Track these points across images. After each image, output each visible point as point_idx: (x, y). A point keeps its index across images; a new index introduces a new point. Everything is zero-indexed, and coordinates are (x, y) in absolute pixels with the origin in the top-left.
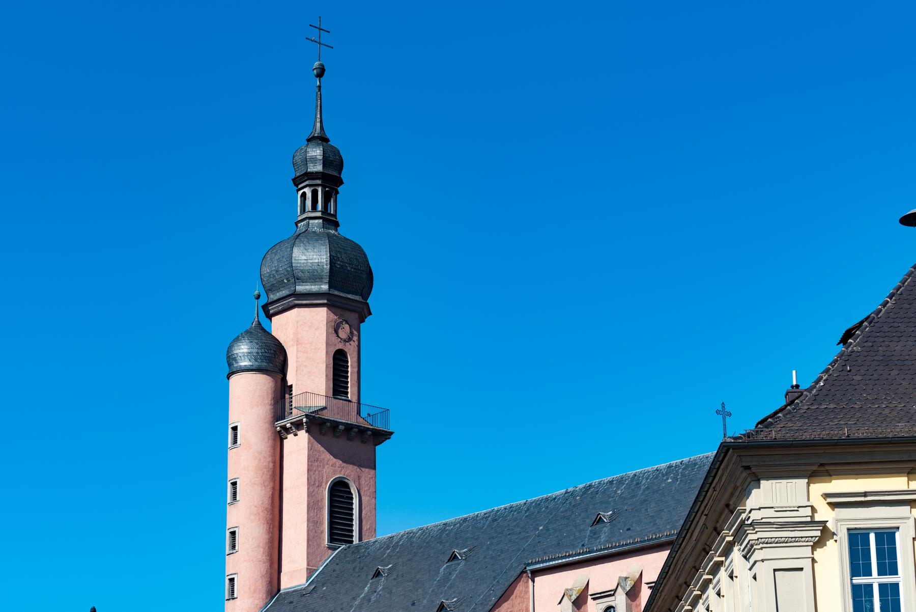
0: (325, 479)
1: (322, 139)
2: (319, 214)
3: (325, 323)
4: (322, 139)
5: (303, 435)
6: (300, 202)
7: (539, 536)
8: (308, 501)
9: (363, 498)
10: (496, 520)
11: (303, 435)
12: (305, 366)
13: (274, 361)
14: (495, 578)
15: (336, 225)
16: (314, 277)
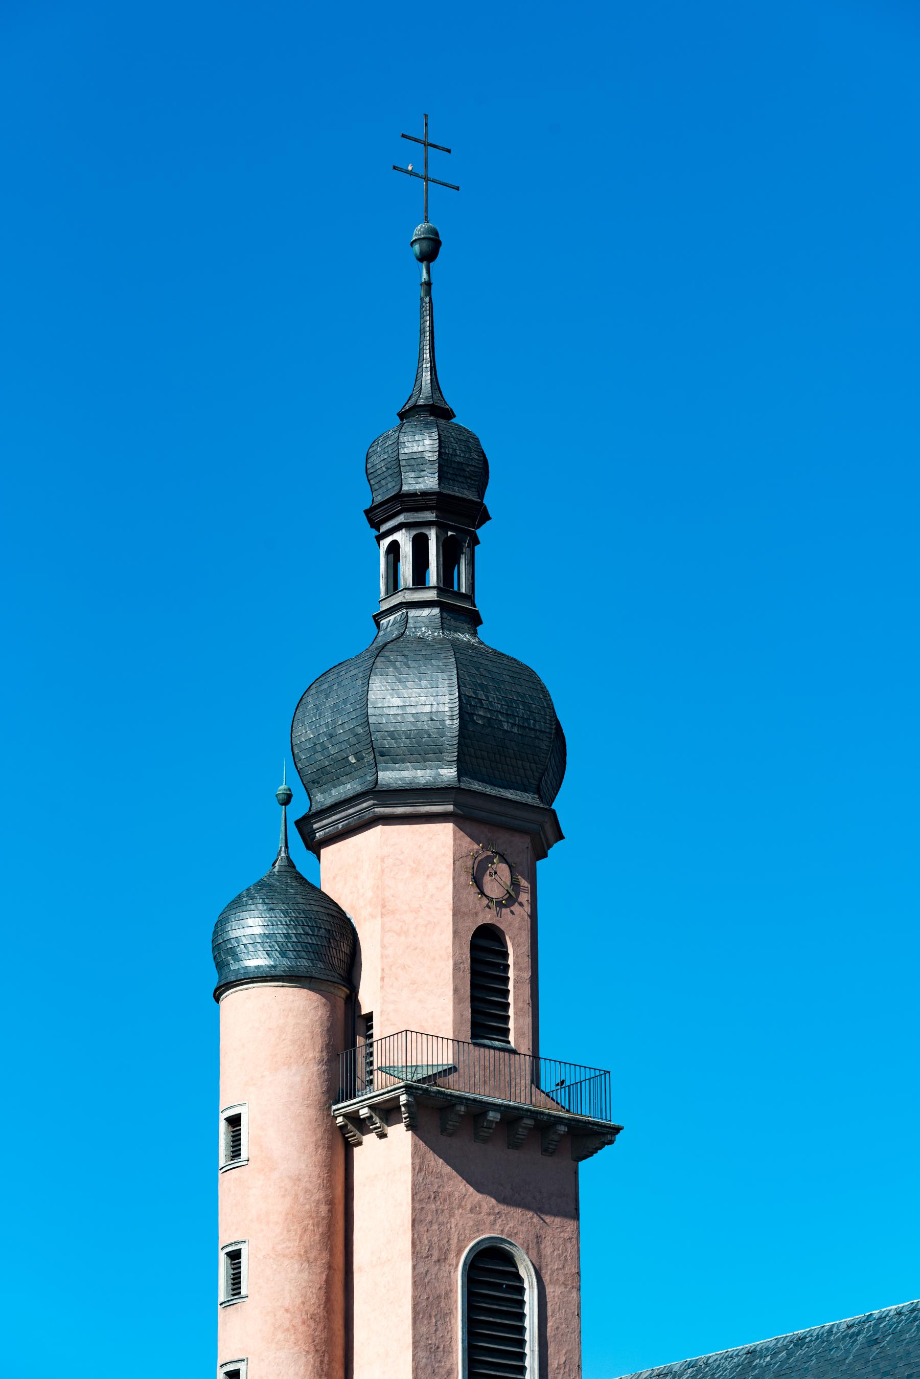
0: (454, 1242)
1: (436, 412)
2: (431, 595)
4: (436, 412)
8: (414, 1297)
9: (549, 1290)
10: (876, 1342)
12: (404, 967)
13: (326, 953)
15: (474, 619)
16: (422, 749)
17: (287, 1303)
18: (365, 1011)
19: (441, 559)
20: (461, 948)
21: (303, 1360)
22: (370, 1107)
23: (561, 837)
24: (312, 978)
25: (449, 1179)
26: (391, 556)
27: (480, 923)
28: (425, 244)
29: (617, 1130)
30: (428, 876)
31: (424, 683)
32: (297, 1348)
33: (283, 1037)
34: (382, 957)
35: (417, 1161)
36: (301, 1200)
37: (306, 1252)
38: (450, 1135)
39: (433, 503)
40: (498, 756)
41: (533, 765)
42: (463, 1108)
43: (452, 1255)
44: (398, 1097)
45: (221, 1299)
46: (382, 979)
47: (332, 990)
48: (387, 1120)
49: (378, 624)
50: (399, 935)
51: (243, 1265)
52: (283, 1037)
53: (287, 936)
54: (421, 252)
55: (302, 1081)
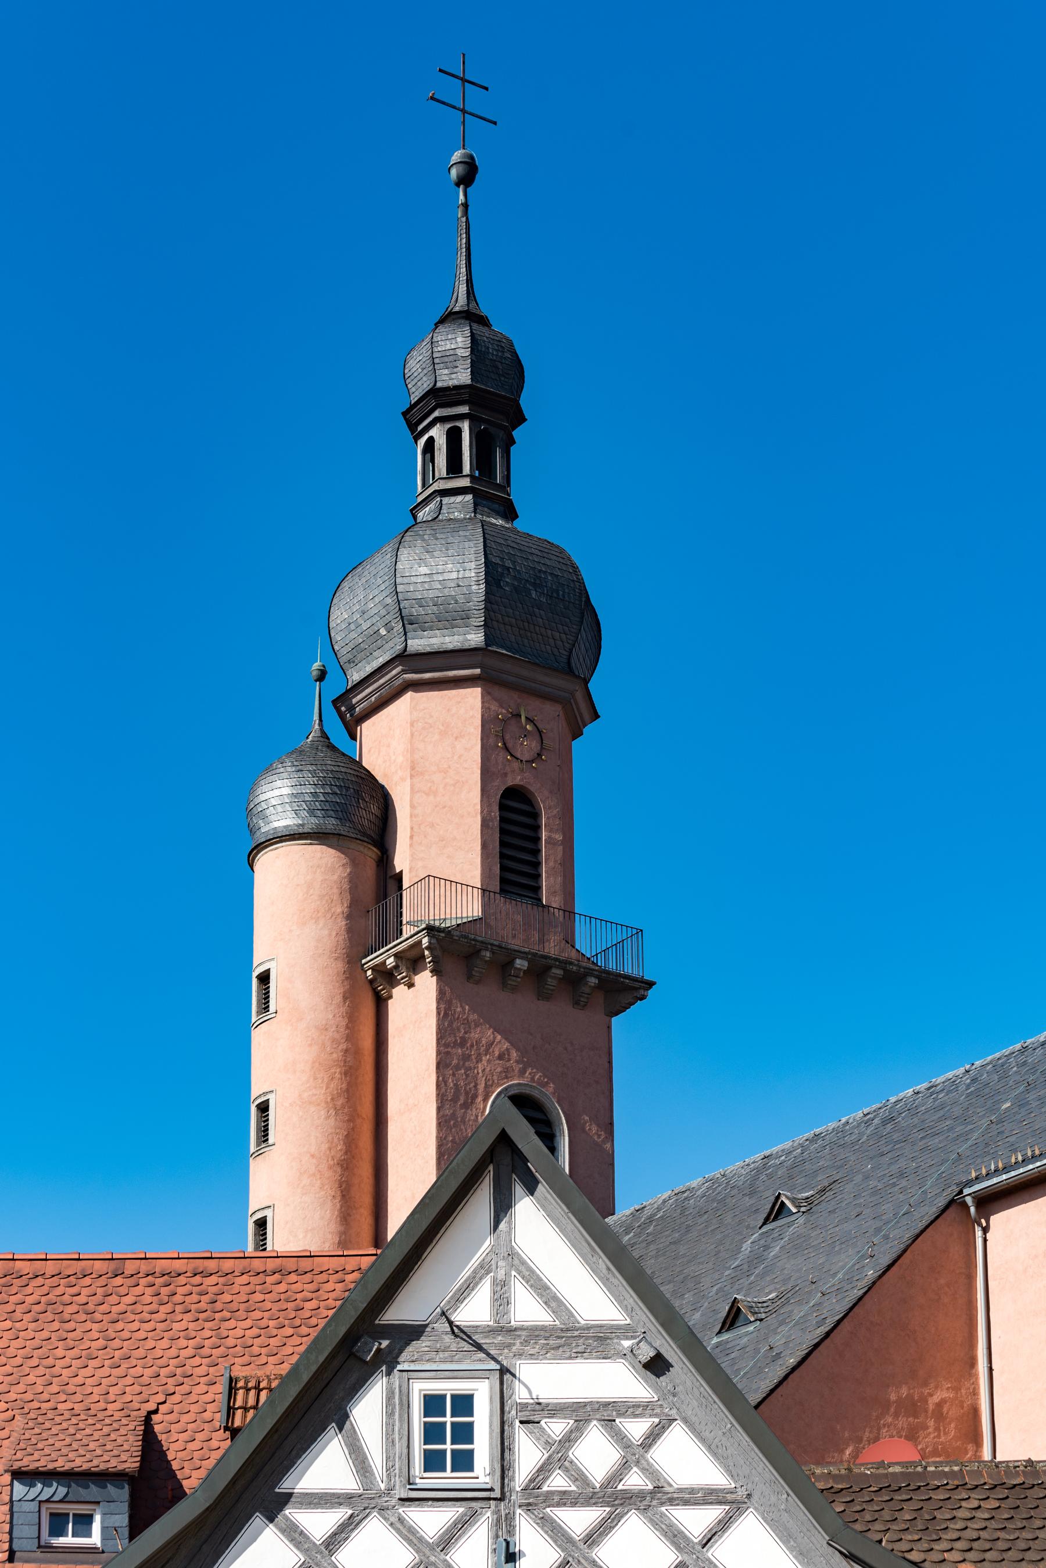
0: (481, 1087)
1: (472, 317)
2: (465, 482)
3: (478, 722)
4: (472, 317)
5: (426, 982)
6: (423, 463)
7: (1000, 1121)
10: (892, 1119)
11: (426, 982)
12: (432, 825)
13: (358, 817)
14: (878, 1230)
15: (509, 512)
16: (450, 616)
17: (313, 1149)
18: (398, 871)
19: (474, 450)
20: (490, 805)
21: (329, 1204)
22: (396, 955)
23: (596, 716)
24: (340, 835)
25: (476, 1026)
26: (428, 456)
27: (510, 783)
28: (461, 167)
29: (651, 984)
30: (456, 738)
31: (450, 552)
32: (323, 1193)
33: (311, 891)
34: (411, 816)
35: (442, 1006)
36: (328, 1049)
37: (332, 1099)
38: (477, 983)
39: (466, 397)
40: (526, 624)
41: (563, 636)
42: (488, 954)
43: (480, 1099)
44: (420, 942)
45: (252, 1150)
46: (411, 837)
47: (362, 849)
48: (414, 969)
49: (415, 517)
50: (428, 794)
51: (270, 1117)
52: (311, 891)
53: (314, 794)
54: (458, 177)
55: (330, 935)
